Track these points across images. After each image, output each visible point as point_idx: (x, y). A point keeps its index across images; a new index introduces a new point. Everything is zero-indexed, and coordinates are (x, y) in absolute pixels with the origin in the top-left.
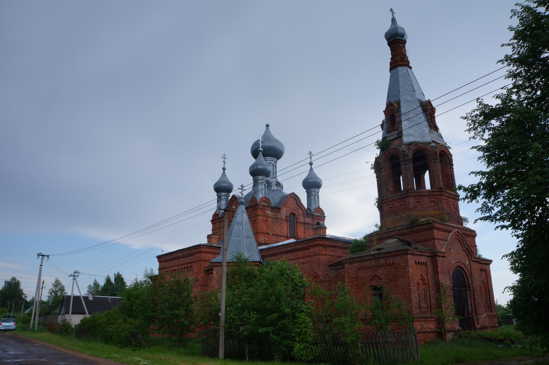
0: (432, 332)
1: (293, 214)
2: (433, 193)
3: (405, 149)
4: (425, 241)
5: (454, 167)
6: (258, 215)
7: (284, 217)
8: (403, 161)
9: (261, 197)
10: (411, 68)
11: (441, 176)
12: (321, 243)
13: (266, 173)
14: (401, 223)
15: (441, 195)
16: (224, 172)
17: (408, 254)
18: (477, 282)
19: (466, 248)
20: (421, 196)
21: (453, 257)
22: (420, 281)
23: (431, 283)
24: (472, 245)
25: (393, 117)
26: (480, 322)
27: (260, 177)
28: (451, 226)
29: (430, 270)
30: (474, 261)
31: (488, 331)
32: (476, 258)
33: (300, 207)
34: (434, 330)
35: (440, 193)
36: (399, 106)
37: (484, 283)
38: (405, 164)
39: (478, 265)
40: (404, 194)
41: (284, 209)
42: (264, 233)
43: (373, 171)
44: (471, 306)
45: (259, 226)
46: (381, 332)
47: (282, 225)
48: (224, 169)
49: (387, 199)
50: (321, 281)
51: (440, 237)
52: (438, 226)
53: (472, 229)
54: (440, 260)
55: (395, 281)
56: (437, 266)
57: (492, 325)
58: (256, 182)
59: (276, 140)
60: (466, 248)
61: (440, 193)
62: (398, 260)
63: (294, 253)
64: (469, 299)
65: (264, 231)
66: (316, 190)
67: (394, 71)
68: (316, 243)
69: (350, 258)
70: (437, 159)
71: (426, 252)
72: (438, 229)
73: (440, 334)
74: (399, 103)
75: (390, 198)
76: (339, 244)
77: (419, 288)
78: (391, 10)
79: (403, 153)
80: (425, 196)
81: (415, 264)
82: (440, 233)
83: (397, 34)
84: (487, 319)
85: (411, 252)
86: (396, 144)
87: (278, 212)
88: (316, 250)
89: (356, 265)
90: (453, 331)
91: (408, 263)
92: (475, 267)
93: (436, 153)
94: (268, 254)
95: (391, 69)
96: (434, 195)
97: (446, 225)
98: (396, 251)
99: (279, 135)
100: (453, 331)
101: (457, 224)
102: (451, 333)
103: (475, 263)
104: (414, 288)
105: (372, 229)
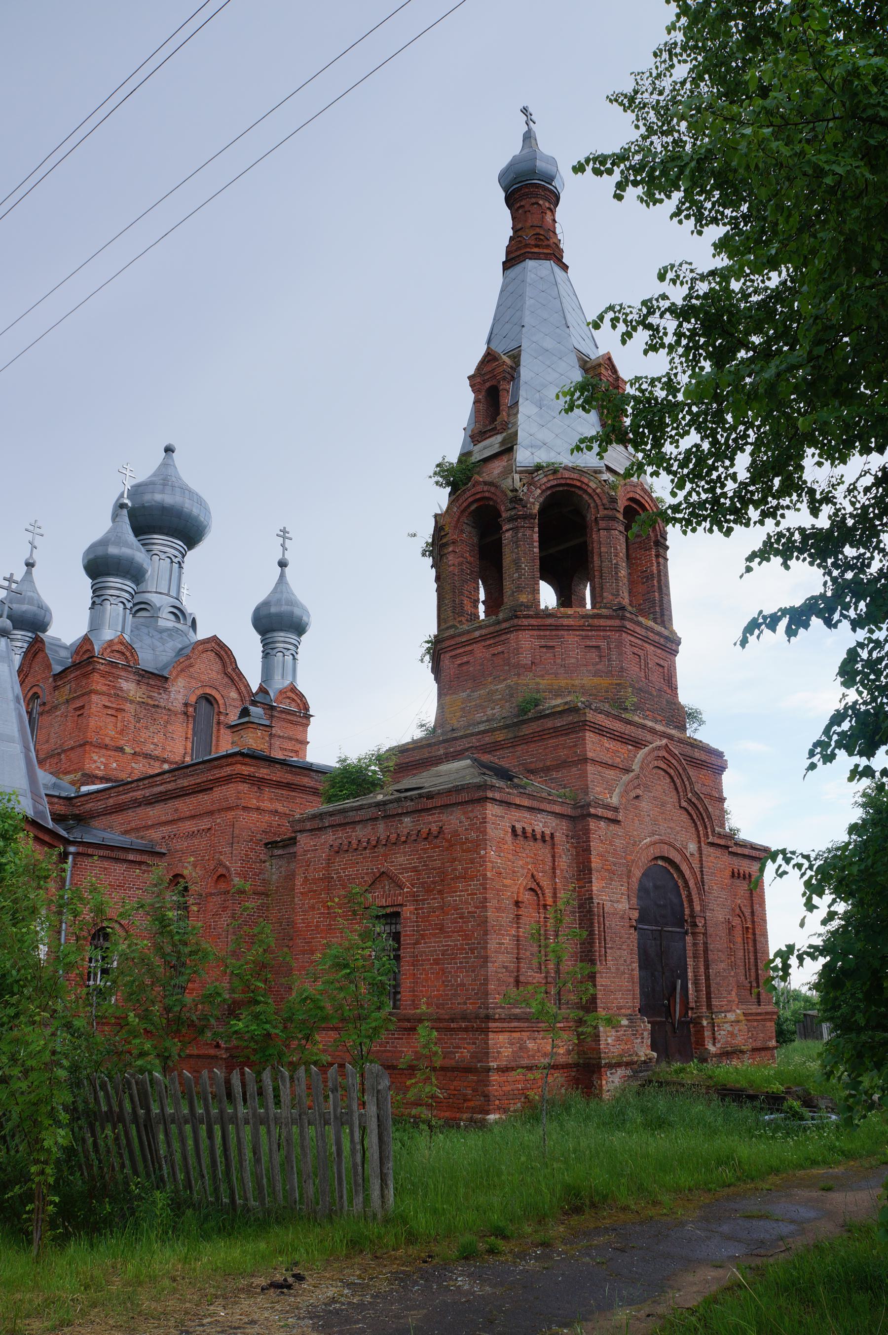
0: (555, 1067)
1: (209, 700)
2: (596, 622)
3: (518, 484)
4: (558, 767)
5: (669, 554)
7: (178, 706)
8: (511, 519)
10: (565, 268)
11: (623, 573)
12: (246, 770)
14: (489, 712)
15: (621, 629)
17: (486, 799)
18: (717, 908)
19: (689, 801)
20: (557, 628)
21: (640, 827)
22: (527, 897)
24: (710, 796)
25: (494, 386)
26: (721, 1034)
27: (114, 581)
28: (644, 727)
29: (564, 861)
30: (712, 844)
32: (720, 836)
33: (232, 680)
34: (562, 1060)
36: (518, 364)
37: (741, 915)
38: (515, 529)
39: (727, 858)
40: (505, 621)
41: (181, 683)
42: (106, 747)
43: (429, 561)
44: (696, 983)
46: (243, 1074)
47: (170, 728)
49: (452, 637)
51: (607, 758)
52: (601, 719)
53: (714, 745)
54: (599, 830)
55: (440, 892)
56: (588, 850)
57: (759, 1044)
58: (99, 596)
59: (185, 489)
60: (689, 801)
61: (616, 623)
62: (454, 820)
63: (171, 804)
64: (690, 962)
65: (107, 741)
66: (292, 637)
67: (512, 272)
68: (228, 770)
69: (314, 817)
70: (614, 518)
71: (555, 802)
72: (600, 731)
73: (586, 1070)
74: (516, 356)
76: (306, 781)
77: (518, 917)
78: (525, 111)
79: (510, 494)
80: (569, 628)
81: (509, 837)
82: (608, 744)
83: (533, 172)
84: (743, 1026)
85: (497, 796)
86: (496, 472)
89: (329, 838)
90: (628, 1064)
91: (484, 832)
92: (717, 864)
93: (613, 500)
94: (100, 805)
95: (508, 265)
96: (598, 628)
97: (629, 722)
98: (449, 792)
99: (202, 481)
100: (628, 1064)
102: (620, 1072)
103: (718, 852)
104: (499, 916)
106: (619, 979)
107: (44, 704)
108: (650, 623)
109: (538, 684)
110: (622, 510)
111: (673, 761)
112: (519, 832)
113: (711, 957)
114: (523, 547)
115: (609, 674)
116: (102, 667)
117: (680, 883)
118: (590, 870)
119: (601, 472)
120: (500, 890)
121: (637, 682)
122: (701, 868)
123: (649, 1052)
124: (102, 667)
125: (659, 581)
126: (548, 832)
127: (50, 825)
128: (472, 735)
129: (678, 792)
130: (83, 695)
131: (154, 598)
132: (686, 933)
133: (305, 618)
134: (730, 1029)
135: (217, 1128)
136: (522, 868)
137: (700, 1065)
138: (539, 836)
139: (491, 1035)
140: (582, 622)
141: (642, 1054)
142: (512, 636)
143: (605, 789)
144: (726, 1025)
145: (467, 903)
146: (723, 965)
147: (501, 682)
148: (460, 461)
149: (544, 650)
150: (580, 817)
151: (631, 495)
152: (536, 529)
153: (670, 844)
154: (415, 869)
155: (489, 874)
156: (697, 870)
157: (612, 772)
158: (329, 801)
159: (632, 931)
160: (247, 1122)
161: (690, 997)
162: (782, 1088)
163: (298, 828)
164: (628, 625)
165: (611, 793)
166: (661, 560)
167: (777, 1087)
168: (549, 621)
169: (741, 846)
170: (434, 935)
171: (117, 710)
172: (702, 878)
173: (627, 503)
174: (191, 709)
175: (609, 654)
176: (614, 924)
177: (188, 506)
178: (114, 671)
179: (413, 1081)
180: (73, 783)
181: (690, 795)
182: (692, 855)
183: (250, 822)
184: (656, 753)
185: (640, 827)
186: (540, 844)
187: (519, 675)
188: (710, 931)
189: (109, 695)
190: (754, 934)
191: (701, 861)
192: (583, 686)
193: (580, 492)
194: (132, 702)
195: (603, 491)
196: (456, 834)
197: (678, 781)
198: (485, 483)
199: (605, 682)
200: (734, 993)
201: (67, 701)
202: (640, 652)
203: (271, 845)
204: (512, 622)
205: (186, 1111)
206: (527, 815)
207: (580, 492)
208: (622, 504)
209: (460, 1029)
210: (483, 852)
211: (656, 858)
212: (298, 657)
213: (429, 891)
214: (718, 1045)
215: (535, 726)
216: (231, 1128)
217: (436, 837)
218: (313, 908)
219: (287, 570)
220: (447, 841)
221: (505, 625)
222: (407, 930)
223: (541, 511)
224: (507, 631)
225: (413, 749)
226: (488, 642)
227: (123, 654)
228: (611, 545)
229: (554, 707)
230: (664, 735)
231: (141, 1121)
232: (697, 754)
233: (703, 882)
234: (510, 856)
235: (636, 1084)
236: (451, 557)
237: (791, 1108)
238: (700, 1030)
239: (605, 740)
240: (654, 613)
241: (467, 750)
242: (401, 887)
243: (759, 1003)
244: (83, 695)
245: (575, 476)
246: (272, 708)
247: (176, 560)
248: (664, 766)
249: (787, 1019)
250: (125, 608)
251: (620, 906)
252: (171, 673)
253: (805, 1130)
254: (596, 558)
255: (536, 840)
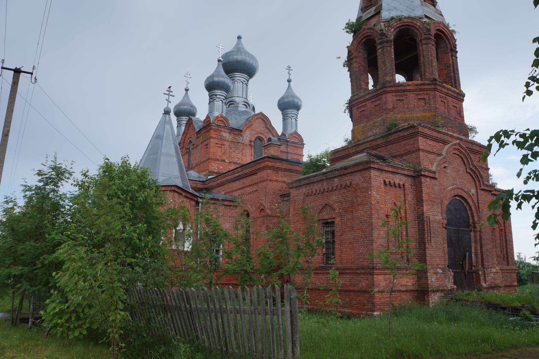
0: (407, 291)
2: (423, 87)
3: (383, 27)
4: (406, 154)
5: (458, 55)
6: (210, 138)
7: (247, 142)
8: (381, 43)
9: (216, 115)
11: (435, 64)
12: (270, 164)
13: (226, 88)
14: (374, 131)
15: (435, 90)
16: (187, 93)
17: (371, 168)
19: (471, 169)
20: (404, 91)
21: (447, 181)
23: (411, 216)
24: (482, 167)
26: (489, 278)
27: (218, 92)
28: (447, 134)
29: (410, 197)
30: (483, 190)
31: (502, 291)
32: (487, 186)
33: (270, 130)
34: (410, 288)
35: (433, 87)
40: (380, 89)
42: (218, 160)
43: (347, 69)
44: (476, 254)
45: (211, 151)
47: (244, 151)
48: (187, 90)
49: (357, 99)
50: (268, 215)
52: (426, 131)
54: (426, 182)
55: (352, 212)
56: (421, 192)
57: (508, 284)
58: (212, 98)
59: (246, 53)
60: (471, 169)
61: (433, 87)
62: (357, 179)
63: (242, 181)
65: (218, 157)
66: (294, 111)
68: (262, 165)
69: (297, 181)
70: (430, 39)
71: (404, 169)
72: (426, 136)
73: (421, 293)
75: (360, 98)
80: (410, 91)
81: (382, 186)
82: (430, 142)
84: (500, 275)
85: (376, 166)
87: (238, 135)
88: (263, 174)
89: (304, 190)
90: (442, 291)
91: (370, 183)
92: (486, 199)
93: (429, 30)
94: (215, 183)
96: (424, 90)
99: (253, 49)
100: (442, 291)
101: (459, 134)
102: (438, 294)
103: (486, 194)
104: (377, 222)
105: (340, 144)
106: (438, 251)
107: (194, 145)
108: (449, 87)
109: (396, 117)
110: (433, 35)
111: (463, 151)
112: (387, 183)
113: (483, 242)
114: (387, 56)
115: (430, 111)
116: (214, 127)
117: (468, 207)
118: (422, 201)
119: (422, 18)
120: (380, 210)
121: (444, 114)
122: (478, 200)
123: (452, 285)
124: (214, 127)
125: (453, 68)
126: (401, 183)
127: (191, 190)
128: (367, 142)
129: (465, 165)
130: (207, 139)
131: (237, 100)
132: (471, 231)
133: (299, 103)
134: (493, 276)
135: (219, 315)
136: (390, 200)
137: (478, 293)
138: (397, 185)
139: (375, 276)
140: (416, 88)
141: (449, 286)
142: (383, 96)
143: (431, 164)
144: (491, 274)
145: (363, 216)
146: (489, 246)
147: (379, 117)
148: (357, 20)
149: (399, 102)
150: (417, 176)
151: (438, 28)
152: (393, 47)
153: (462, 190)
154: (340, 202)
155: (373, 202)
156: (476, 202)
157: (432, 156)
158: (305, 175)
159: (444, 229)
160: (231, 313)
161: (473, 261)
162: (520, 305)
163: (290, 186)
164: (438, 88)
165: (432, 165)
166: (454, 58)
167: (517, 304)
168: (400, 88)
169: (498, 191)
170: (349, 231)
171: (222, 145)
172: (478, 205)
173: (436, 32)
174: (253, 143)
175: (429, 102)
176: (434, 226)
177: (248, 59)
178: (219, 128)
179: (328, 296)
180: (205, 175)
181: (471, 166)
182: (473, 194)
183: (273, 186)
184: (454, 147)
185: (447, 181)
186: (398, 189)
187: (387, 113)
188: (483, 230)
189: (218, 139)
190: (505, 233)
191: (478, 197)
192: (417, 117)
193: (413, 28)
194: (227, 141)
195: (424, 27)
196: (357, 185)
197: (465, 160)
198: (368, 29)
199: (428, 114)
200: (495, 260)
201: (202, 142)
202: (445, 100)
203: (282, 196)
204: (383, 90)
205: (206, 307)
206: (391, 175)
207: (413, 28)
208: (433, 32)
209: (361, 273)
210: (370, 192)
211: (455, 196)
212: (298, 119)
213: (346, 211)
214: (487, 283)
215: (395, 136)
216: (225, 316)
217: (349, 187)
218: (297, 221)
219: (291, 83)
220: (354, 188)
221: (380, 92)
222: (337, 229)
223: (395, 40)
224: (381, 94)
225: (341, 151)
226: (373, 100)
227: (223, 121)
228: (428, 52)
229: (403, 126)
230: (457, 138)
231: (188, 310)
232: (474, 147)
233: (479, 207)
234: (383, 194)
235: (445, 300)
236: (355, 64)
237: (524, 315)
238: (478, 276)
239: (428, 141)
240: (451, 83)
241: (365, 149)
242: (334, 210)
243: (508, 264)
244: (207, 139)
245: (410, 21)
246: (287, 141)
247: (244, 83)
248: (458, 153)
249: (523, 274)
250: (223, 103)
251: (438, 218)
252: (243, 128)
253: (532, 326)
254: (421, 58)
255: (396, 187)
